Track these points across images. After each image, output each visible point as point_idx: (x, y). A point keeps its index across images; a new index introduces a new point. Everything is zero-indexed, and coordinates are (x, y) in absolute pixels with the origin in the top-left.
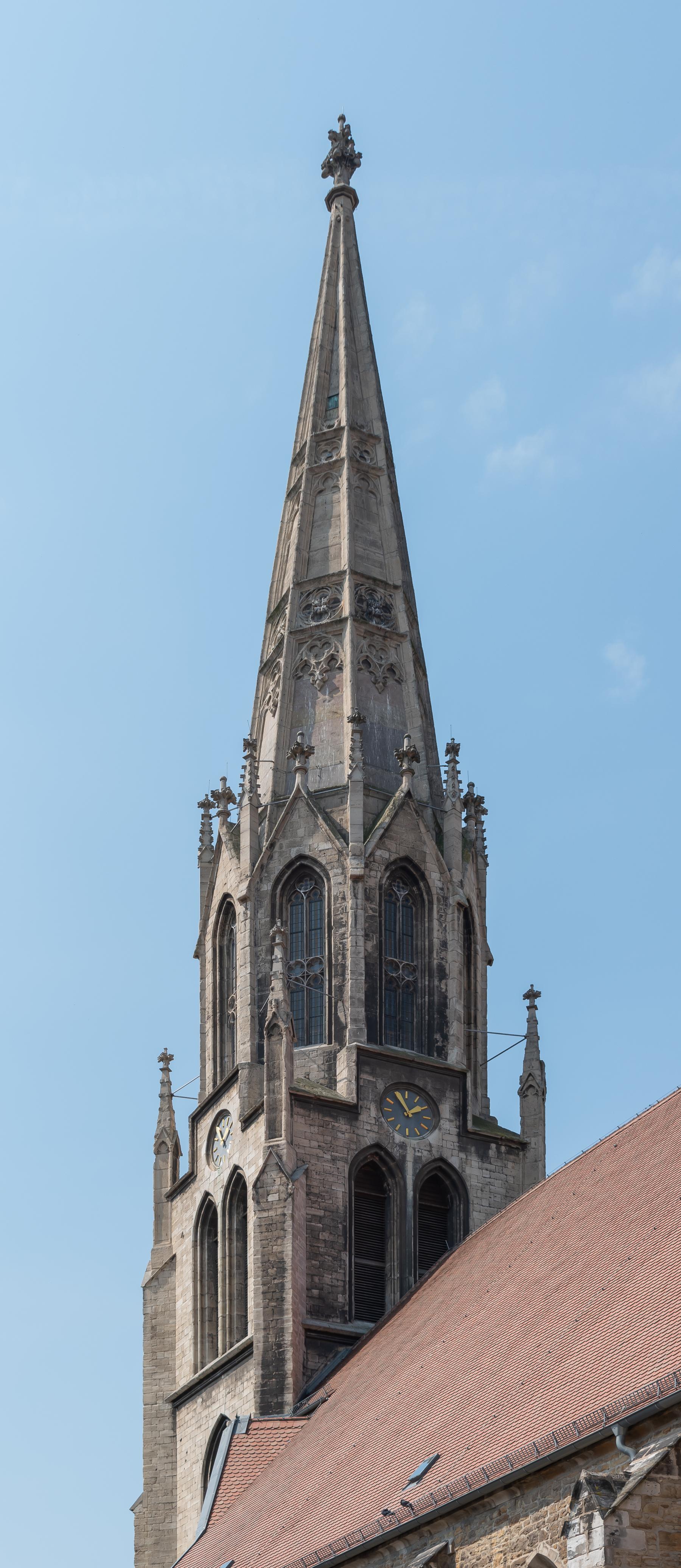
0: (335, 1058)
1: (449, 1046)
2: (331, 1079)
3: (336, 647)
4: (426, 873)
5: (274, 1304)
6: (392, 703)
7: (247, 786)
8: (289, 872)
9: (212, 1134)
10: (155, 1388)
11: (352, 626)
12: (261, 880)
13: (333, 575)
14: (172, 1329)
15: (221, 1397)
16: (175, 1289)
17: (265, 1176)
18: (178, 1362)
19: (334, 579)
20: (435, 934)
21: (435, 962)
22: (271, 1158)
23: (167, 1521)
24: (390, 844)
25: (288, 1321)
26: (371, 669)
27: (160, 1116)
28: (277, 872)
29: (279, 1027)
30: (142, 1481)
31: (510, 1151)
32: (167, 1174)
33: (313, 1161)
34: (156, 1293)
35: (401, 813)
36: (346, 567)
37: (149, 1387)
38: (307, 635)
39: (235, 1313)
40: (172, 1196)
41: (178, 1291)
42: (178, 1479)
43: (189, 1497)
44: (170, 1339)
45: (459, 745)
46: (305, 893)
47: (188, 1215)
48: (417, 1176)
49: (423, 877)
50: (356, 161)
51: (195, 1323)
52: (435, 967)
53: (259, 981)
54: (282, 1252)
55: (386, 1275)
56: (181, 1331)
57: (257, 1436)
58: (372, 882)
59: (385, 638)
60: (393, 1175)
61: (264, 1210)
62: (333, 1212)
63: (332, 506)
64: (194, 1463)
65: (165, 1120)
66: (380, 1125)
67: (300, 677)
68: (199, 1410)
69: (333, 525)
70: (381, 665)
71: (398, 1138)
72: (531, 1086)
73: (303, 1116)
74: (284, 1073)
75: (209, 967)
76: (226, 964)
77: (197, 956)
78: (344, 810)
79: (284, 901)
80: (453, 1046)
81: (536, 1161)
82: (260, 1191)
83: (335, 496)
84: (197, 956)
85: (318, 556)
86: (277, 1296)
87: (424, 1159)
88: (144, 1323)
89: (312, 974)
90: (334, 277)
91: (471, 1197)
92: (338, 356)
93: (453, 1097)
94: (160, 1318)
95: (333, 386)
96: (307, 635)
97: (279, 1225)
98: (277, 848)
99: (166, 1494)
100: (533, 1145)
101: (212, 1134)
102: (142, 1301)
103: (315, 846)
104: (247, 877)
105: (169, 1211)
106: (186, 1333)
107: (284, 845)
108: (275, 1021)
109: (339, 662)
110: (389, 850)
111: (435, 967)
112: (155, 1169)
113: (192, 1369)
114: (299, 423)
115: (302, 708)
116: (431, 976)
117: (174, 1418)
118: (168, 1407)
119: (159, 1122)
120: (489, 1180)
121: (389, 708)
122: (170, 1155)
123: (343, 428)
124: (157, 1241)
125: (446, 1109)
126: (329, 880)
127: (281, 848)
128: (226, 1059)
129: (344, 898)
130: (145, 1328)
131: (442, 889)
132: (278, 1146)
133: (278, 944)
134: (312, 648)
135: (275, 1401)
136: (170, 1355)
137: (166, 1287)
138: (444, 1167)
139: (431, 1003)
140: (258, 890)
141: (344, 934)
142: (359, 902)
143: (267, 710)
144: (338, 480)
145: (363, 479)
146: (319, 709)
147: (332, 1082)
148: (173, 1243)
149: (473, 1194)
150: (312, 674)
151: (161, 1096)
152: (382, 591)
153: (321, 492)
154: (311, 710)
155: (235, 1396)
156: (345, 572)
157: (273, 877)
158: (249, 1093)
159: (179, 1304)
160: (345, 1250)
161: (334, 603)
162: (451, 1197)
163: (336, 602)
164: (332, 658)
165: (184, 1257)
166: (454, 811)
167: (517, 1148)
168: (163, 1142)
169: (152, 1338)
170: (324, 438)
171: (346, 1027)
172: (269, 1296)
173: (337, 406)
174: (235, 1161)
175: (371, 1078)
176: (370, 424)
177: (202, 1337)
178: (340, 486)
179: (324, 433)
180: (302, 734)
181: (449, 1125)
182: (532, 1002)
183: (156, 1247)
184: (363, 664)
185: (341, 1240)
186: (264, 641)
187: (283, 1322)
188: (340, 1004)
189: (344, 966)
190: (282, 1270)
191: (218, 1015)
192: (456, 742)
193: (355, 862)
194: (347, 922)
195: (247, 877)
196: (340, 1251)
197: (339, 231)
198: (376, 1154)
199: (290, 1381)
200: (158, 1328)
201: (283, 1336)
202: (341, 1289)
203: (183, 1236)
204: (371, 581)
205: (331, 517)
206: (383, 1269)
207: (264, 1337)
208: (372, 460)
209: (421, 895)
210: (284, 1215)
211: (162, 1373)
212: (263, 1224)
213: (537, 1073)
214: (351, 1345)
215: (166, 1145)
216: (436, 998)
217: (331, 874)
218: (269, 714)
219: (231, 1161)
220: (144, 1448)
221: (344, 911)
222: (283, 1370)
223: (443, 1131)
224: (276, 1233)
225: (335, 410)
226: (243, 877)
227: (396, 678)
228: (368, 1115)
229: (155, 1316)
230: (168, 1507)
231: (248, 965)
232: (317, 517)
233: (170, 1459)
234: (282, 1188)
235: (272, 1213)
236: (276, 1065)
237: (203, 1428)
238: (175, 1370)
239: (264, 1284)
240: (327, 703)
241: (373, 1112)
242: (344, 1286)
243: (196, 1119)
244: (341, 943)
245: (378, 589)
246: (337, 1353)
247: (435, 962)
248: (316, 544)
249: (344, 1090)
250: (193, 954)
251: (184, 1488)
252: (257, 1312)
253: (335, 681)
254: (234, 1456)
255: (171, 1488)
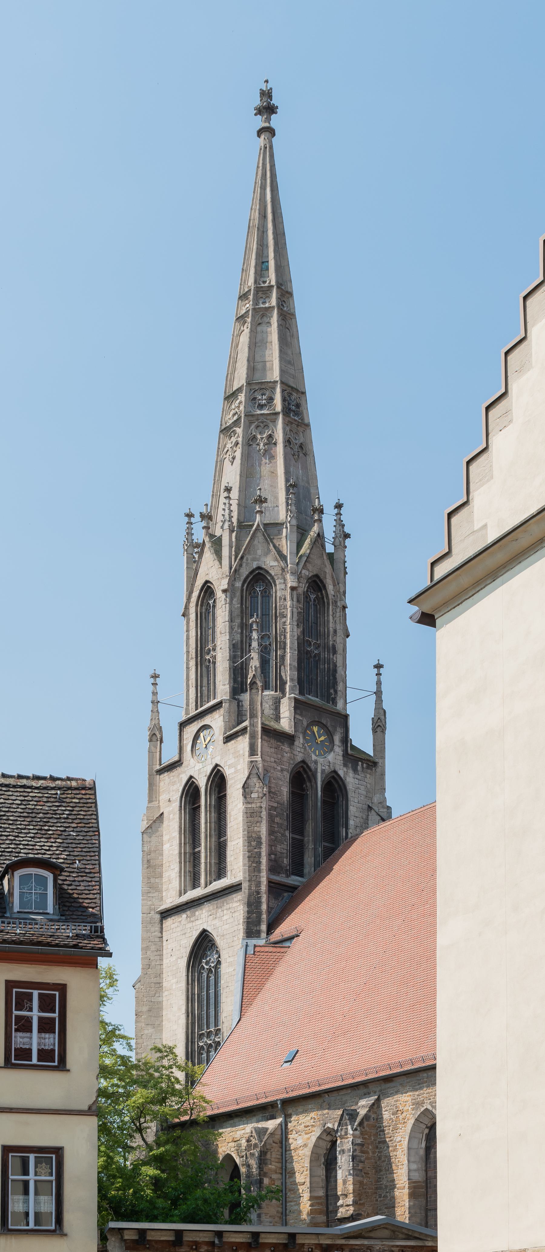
0: (280, 702)
1: (338, 698)
2: (277, 715)
3: (273, 430)
4: (327, 585)
5: (255, 865)
6: (302, 468)
7: (227, 517)
8: (252, 576)
9: (196, 737)
10: (150, 903)
11: (284, 419)
12: (235, 579)
13: (270, 382)
14: (161, 863)
15: (204, 917)
16: (162, 836)
17: (249, 781)
18: (165, 887)
19: (270, 384)
20: (331, 625)
21: (331, 643)
22: (254, 769)
23: (156, 995)
24: (310, 566)
25: (263, 877)
26: (291, 446)
27: (152, 715)
28: (245, 576)
29: (256, 684)
30: (141, 966)
31: (369, 767)
32: (156, 756)
33: (272, 771)
34: (150, 837)
35: (314, 548)
36: (278, 379)
37: (145, 902)
38: (255, 419)
39: (213, 861)
40: (160, 772)
41: (165, 838)
42: (164, 967)
43: (175, 980)
44: (159, 870)
45: (343, 504)
46: (260, 591)
47: (175, 787)
48: (323, 781)
49: (324, 586)
50: (275, 110)
51: (180, 862)
52: (331, 646)
53: (234, 645)
54: (259, 832)
55: (305, 845)
56: (168, 865)
57: (260, 957)
58: (300, 590)
59: (298, 426)
60: (310, 781)
61: (249, 803)
62: (281, 804)
63: (267, 336)
64: (179, 958)
65: (155, 719)
66: (305, 749)
67: (251, 445)
68: (183, 922)
69: (268, 348)
70: (296, 444)
71: (314, 757)
72: (379, 726)
73: (267, 741)
74: (259, 714)
75: (193, 624)
76: (204, 625)
77: (184, 615)
78: (281, 538)
79: (247, 594)
80: (340, 698)
81: (382, 775)
82: (247, 790)
83: (269, 329)
84: (184, 615)
85: (259, 366)
86: (256, 860)
87: (326, 771)
88: (143, 857)
89: (264, 644)
90: (263, 184)
91: (349, 797)
92: (267, 236)
93: (340, 731)
94: (153, 855)
95: (264, 255)
96: (255, 419)
97: (258, 813)
98: (244, 560)
99: (156, 977)
100: (380, 764)
101: (196, 737)
102: (141, 842)
103: (268, 562)
104: (227, 576)
105: (158, 782)
106: (172, 867)
107: (249, 559)
108: (254, 680)
109: (274, 440)
110: (308, 570)
111: (331, 646)
112: (149, 752)
113: (178, 894)
114: (242, 272)
115: (253, 466)
116: (328, 652)
117: (162, 925)
118: (158, 917)
119: (152, 719)
120: (358, 786)
121: (300, 472)
122: (159, 742)
123: (272, 286)
124: (150, 801)
125: (337, 739)
126: (275, 585)
127: (247, 560)
128: (204, 688)
129: (285, 599)
130: (143, 862)
131: (334, 596)
132: (256, 761)
133: (255, 630)
134: (257, 427)
135: (255, 929)
136: (159, 881)
137: (157, 834)
138: (336, 776)
139: (329, 668)
140: (233, 585)
141: (285, 622)
142: (295, 603)
143: (225, 458)
144: (270, 319)
145: (283, 319)
146: (263, 468)
147: (277, 718)
148: (160, 804)
149: (351, 794)
150: (258, 445)
151: (153, 702)
152: (295, 394)
153: (259, 324)
154: (258, 468)
155: (216, 918)
156: (277, 382)
157: (243, 578)
158: (229, 719)
159: (166, 847)
160: (287, 830)
161: (270, 399)
162: (338, 795)
163: (271, 399)
164: (270, 436)
165: (171, 816)
166: (340, 547)
167: (372, 765)
168: (154, 734)
169: (148, 868)
170: (262, 290)
171: (286, 683)
172: (252, 859)
173: (267, 269)
174: (217, 761)
175: (300, 718)
176: (286, 283)
177: (185, 872)
178: (272, 323)
179: (262, 287)
180: (260, 489)
181: (338, 749)
182: (379, 671)
183: (149, 806)
184: (288, 442)
185: (285, 823)
186: (223, 412)
187: (260, 878)
188: (282, 667)
189: (285, 643)
190: (259, 843)
191: (199, 658)
192: (341, 502)
193: (292, 577)
194: (287, 615)
195: (227, 576)
196: (285, 830)
197: (266, 154)
198: (302, 767)
199: (264, 916)
200: (151, 861)
201: (260, 886)
202: (285, 855)
203: (169, 801)
204: (290, 389)
205: (267, 342)
206: (302, 841)
207: (249, 886)
208: (287, 307)
209: (323, 598)
210: (261, 807)
211: (154, 893)
212: (248, 812)
213: (383, 717)
214: (293, 892)
215: (156, 736)
216: (331, 666)
217: (277, 582)
218: (227, 463)
219: (213, 760)
220: (142, 944)
221: (285, 607)
222: (260, 909)
223: (336, 753)
224: (256, 819)
225: (267, 271)
226: (224, 576)
227: (304, 452)
228: (299, 741)
229: (149, 854)
230: (158, 985)
231: (228, 634)
232: (257, 340)
233: (158, 953)
234: (260, 790)
235: (254, 805)
236: (255, 708)
237: (187, 935)
238: (162, 891)
239: (249, 852)
240: (267, 465)
241: (301, 740)
242: (287, 853)
243: (183, 725)
244: (283, 628)
245: (293, 393)
246: (284, 897)
247: (331, 643)
248: (258, 358)
249: (286, 723)
250: (182, 614)
251: (169, 974)
252: (245, 869)
253: (272, 452)
254: (249, 969)
255: (159, 972)
